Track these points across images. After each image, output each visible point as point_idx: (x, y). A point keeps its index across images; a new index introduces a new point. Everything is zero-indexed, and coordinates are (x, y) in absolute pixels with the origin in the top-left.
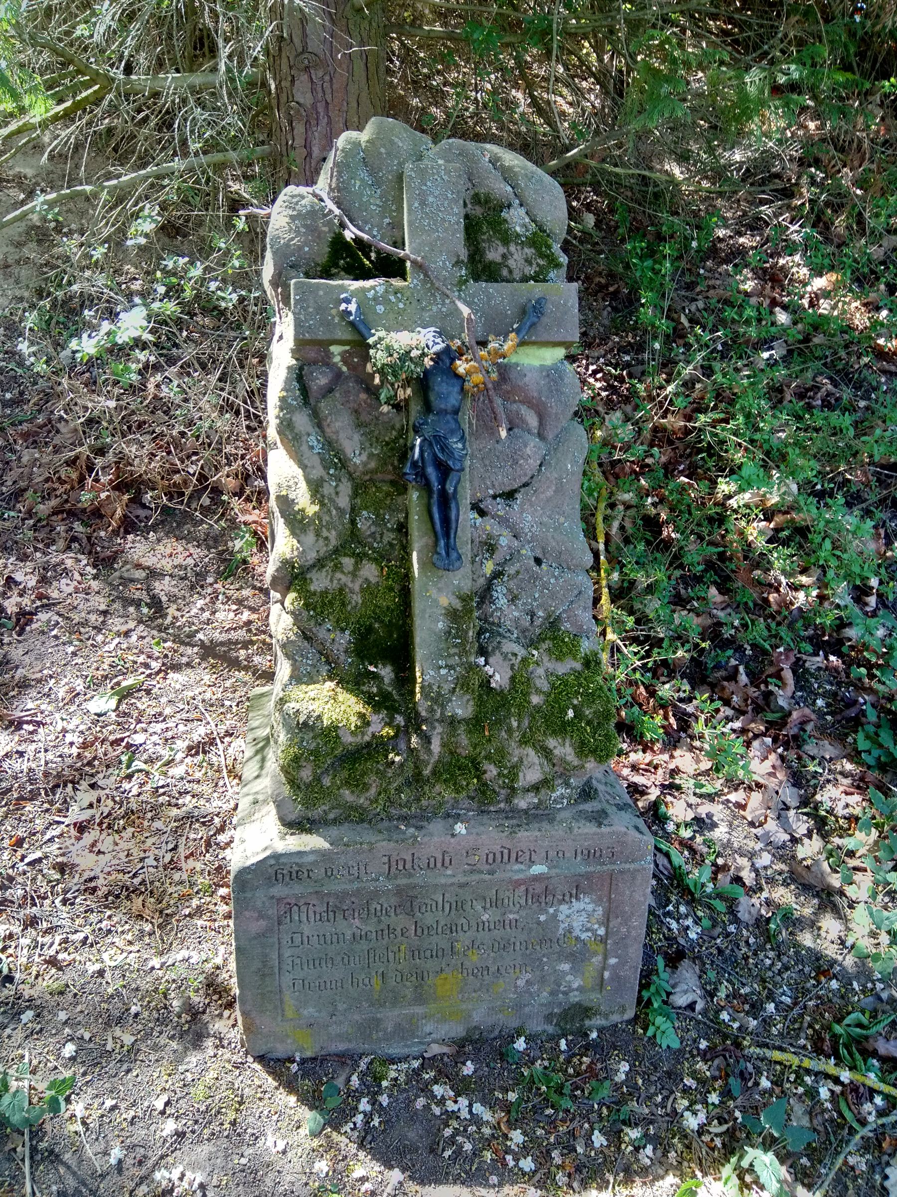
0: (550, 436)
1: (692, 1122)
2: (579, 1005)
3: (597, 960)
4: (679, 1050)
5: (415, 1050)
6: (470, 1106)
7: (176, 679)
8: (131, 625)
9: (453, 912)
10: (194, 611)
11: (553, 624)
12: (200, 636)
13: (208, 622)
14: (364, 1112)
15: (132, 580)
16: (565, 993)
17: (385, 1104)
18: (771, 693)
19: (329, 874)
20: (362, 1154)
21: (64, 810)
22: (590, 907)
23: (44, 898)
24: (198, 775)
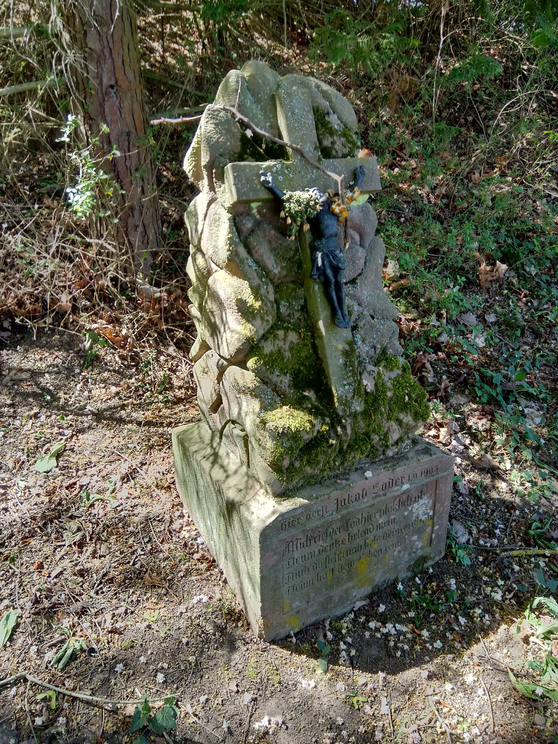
0: (367, 245)
1: (498, 597)
3: (429, 529)
4: (472, 565)
5: (348, 608)
7: (87, 438)
8: (36, 410)
10: (77, 393)
11: (384, 351)
12: (88, 407)
13: (89, 398)
15: (21, 380)
18: (424, 376)
19: (308, 518)
20: (356, 672)
21: (59, 537)
23: (81, 595)
24: (136, 494)
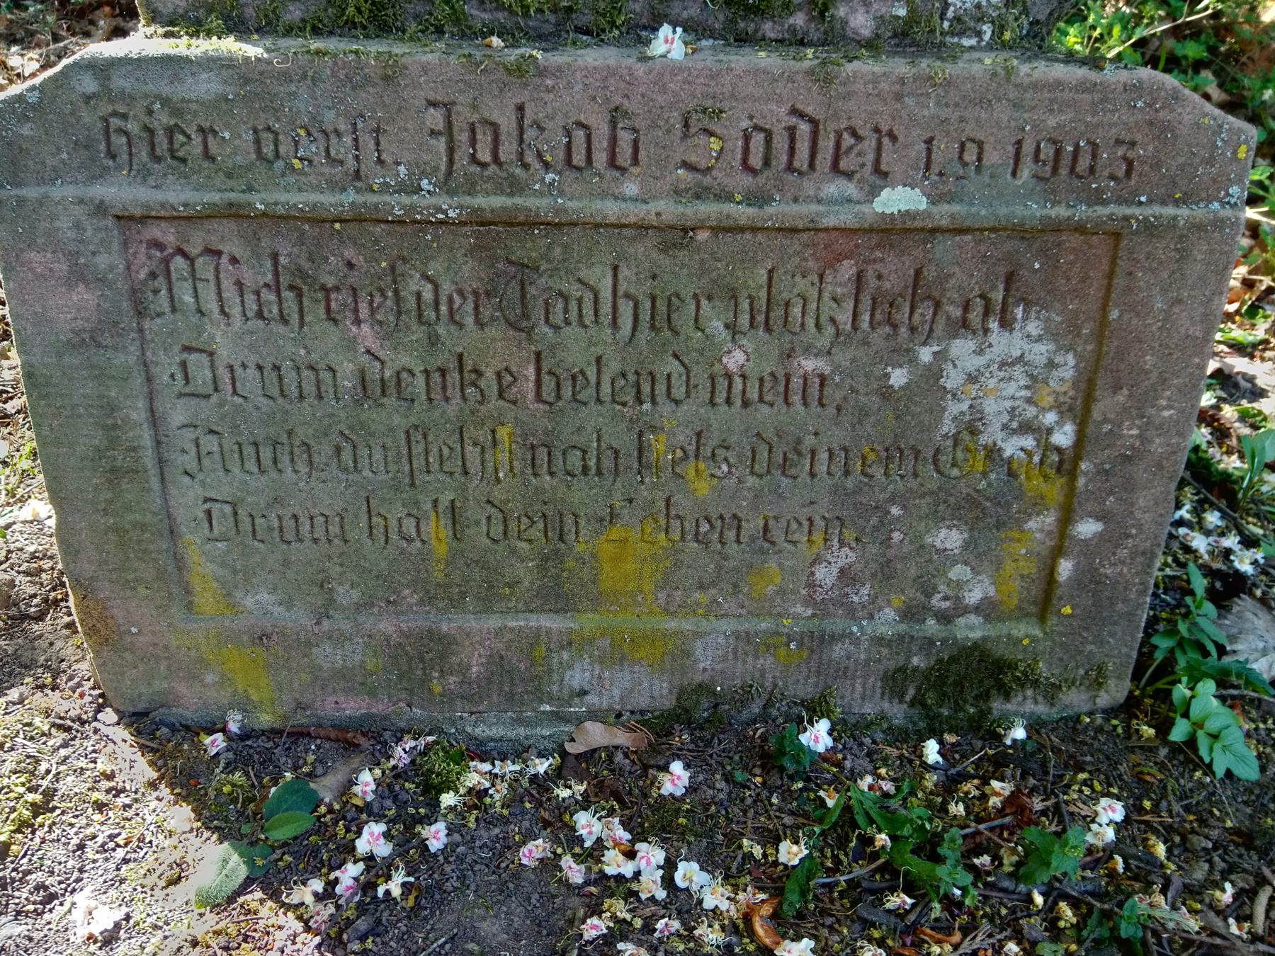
2: (977, 654)
3: (1041, 524)
6: (669, 866)
9: (644, 334)
14: (370, 859)
16: (945, 618)
17: (435, 845)
22: (1040, 352)
